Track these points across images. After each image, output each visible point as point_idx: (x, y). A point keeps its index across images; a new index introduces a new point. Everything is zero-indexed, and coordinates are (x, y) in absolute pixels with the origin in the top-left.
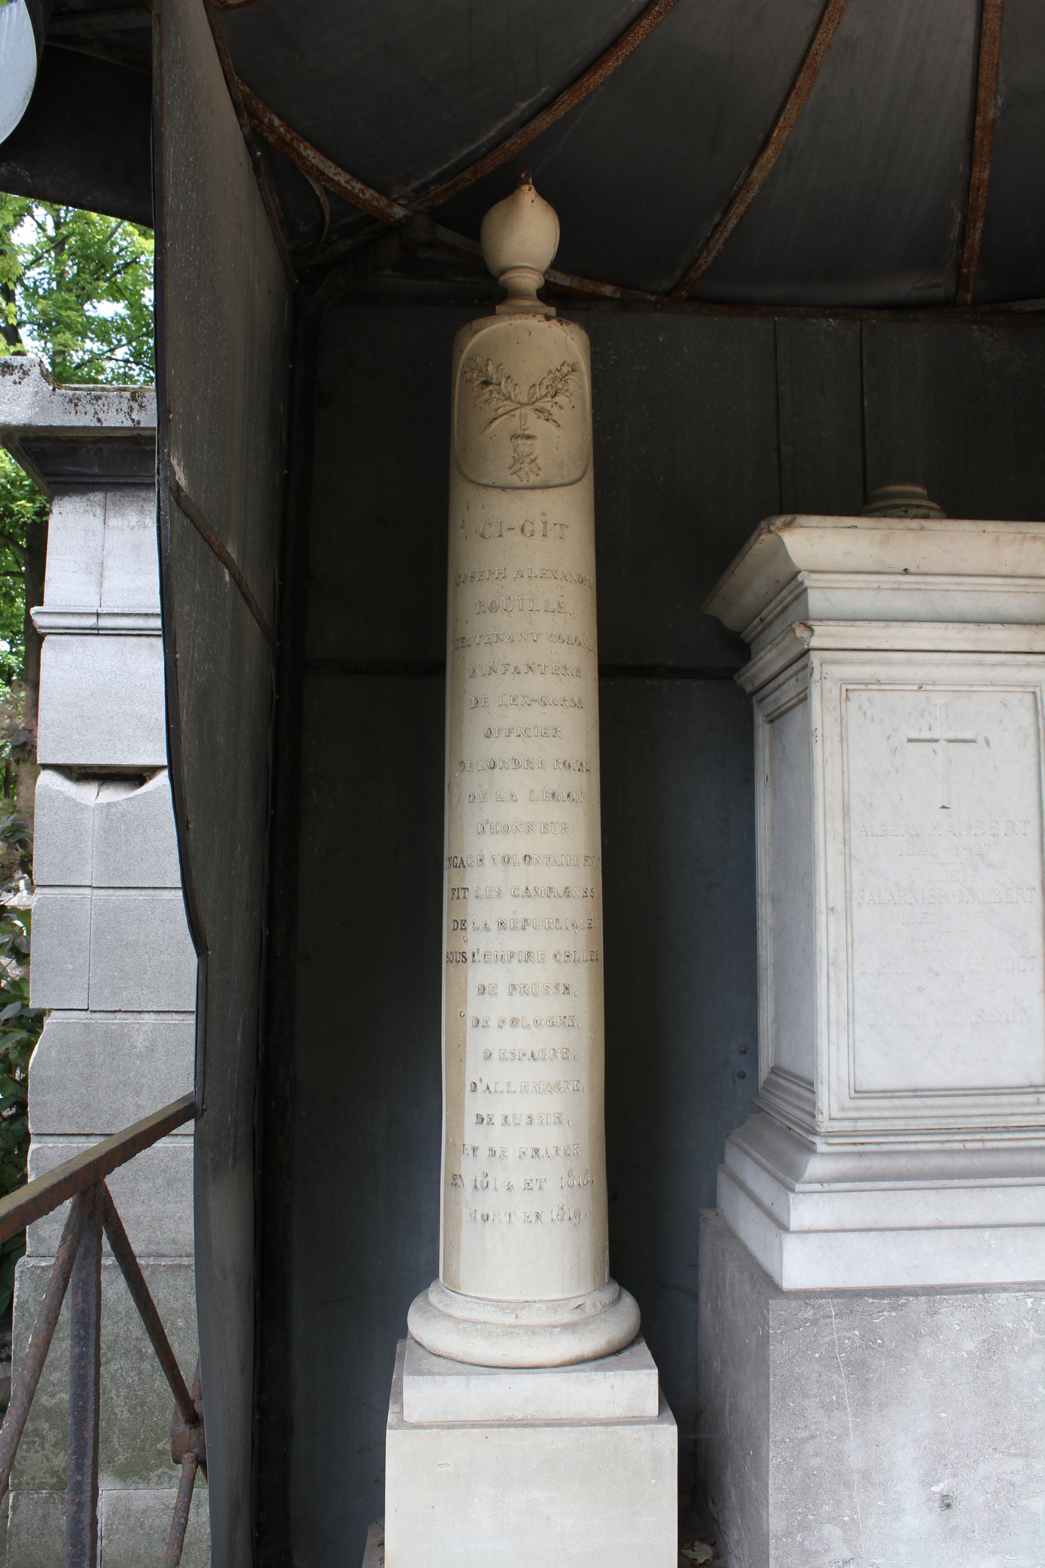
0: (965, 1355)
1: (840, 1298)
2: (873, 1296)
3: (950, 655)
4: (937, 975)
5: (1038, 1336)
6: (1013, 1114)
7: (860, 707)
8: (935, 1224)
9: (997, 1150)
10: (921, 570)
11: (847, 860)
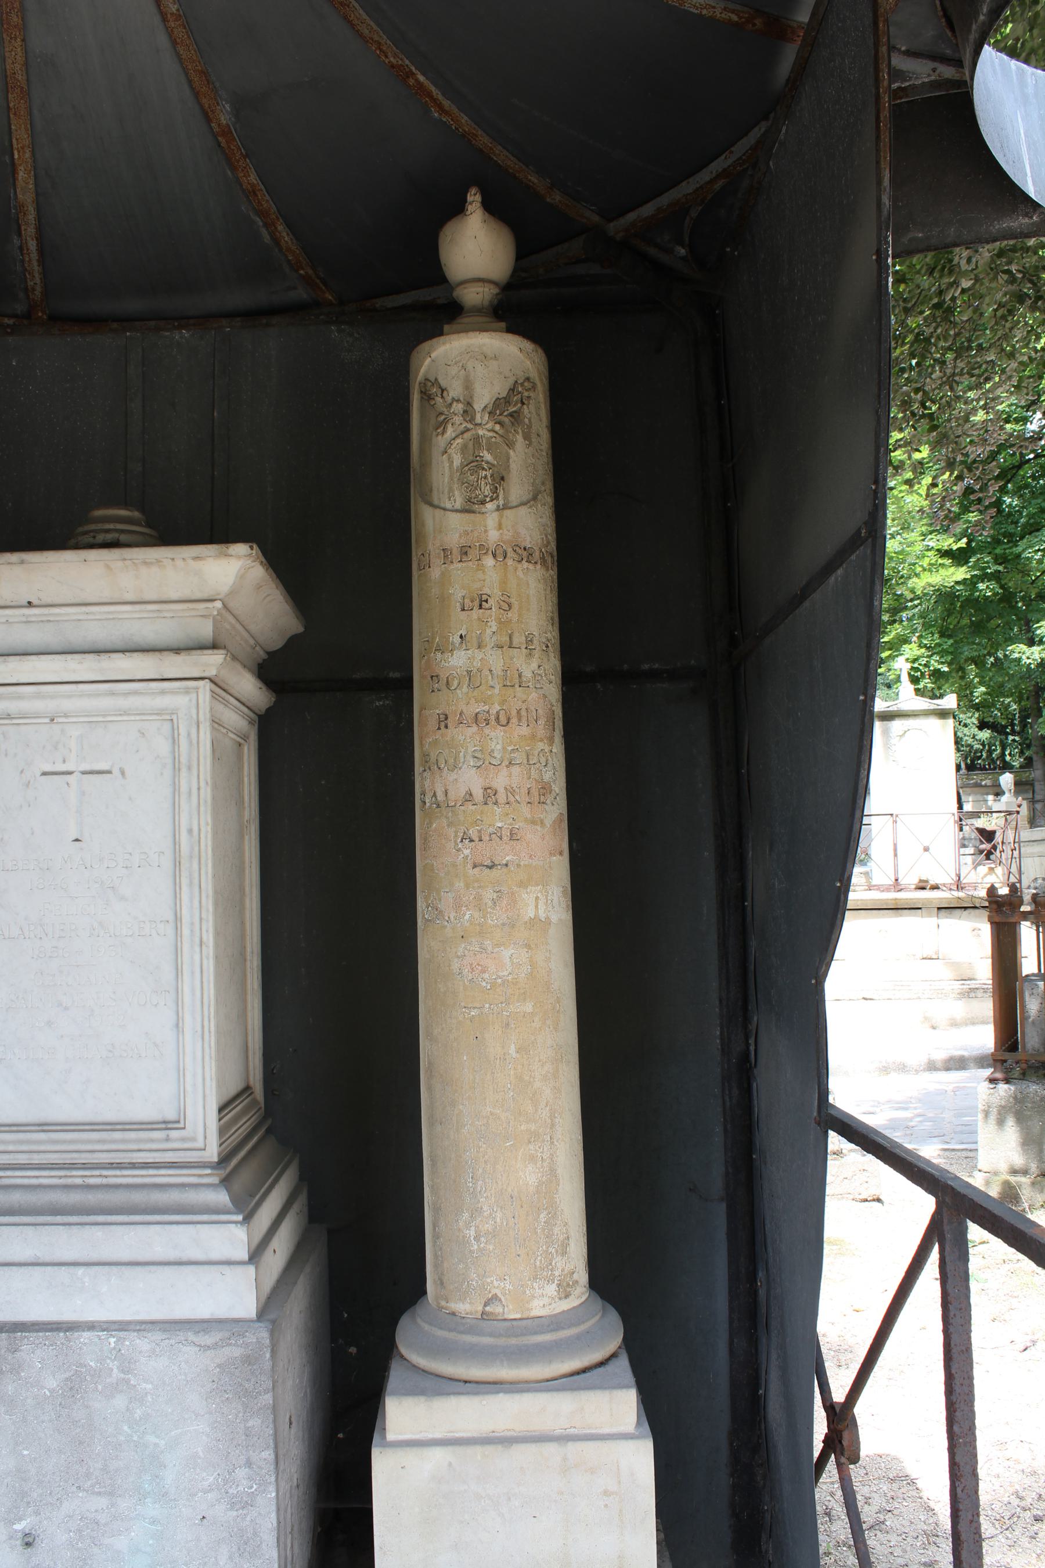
0: (48, 1393)
3: (81, 686)
4: (66, 1009)
5: (122, 1375)
8: (34, 1261)
10: (43, 602)
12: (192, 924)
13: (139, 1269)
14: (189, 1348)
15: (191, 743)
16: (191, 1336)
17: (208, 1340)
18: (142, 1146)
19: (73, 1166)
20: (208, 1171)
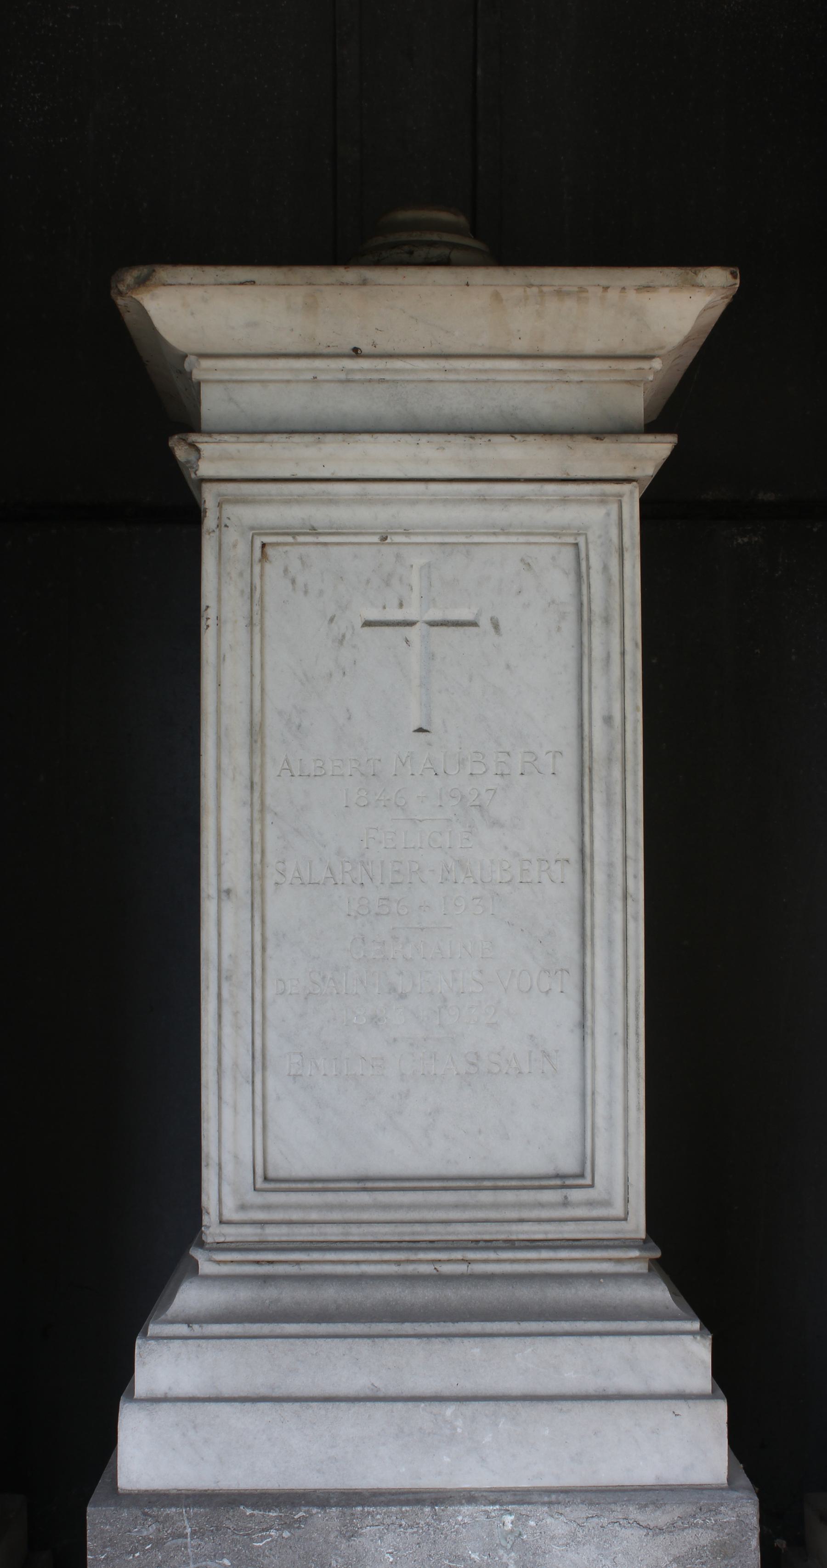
1: (200, 1506)
2: (254, 1506)
4: (403, 996)
6: (521, 1221)
7: (286, 571)
8: (369, 1393)
9: (490, 1277)
10: (379, 350)
11: (256, 815)
12: (611, 865)
13: (543, 1406)
14: (628, 1532)
15: (609, 580)
16: (634, 1513)
17: (661, 1518)
18: (526, 1214)
19: (414, 1245)
20: (635, 1253)
